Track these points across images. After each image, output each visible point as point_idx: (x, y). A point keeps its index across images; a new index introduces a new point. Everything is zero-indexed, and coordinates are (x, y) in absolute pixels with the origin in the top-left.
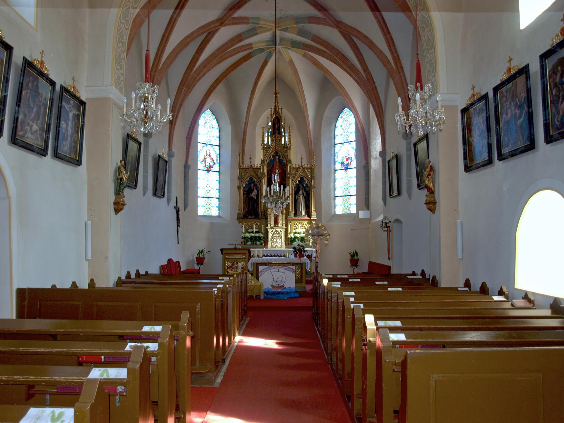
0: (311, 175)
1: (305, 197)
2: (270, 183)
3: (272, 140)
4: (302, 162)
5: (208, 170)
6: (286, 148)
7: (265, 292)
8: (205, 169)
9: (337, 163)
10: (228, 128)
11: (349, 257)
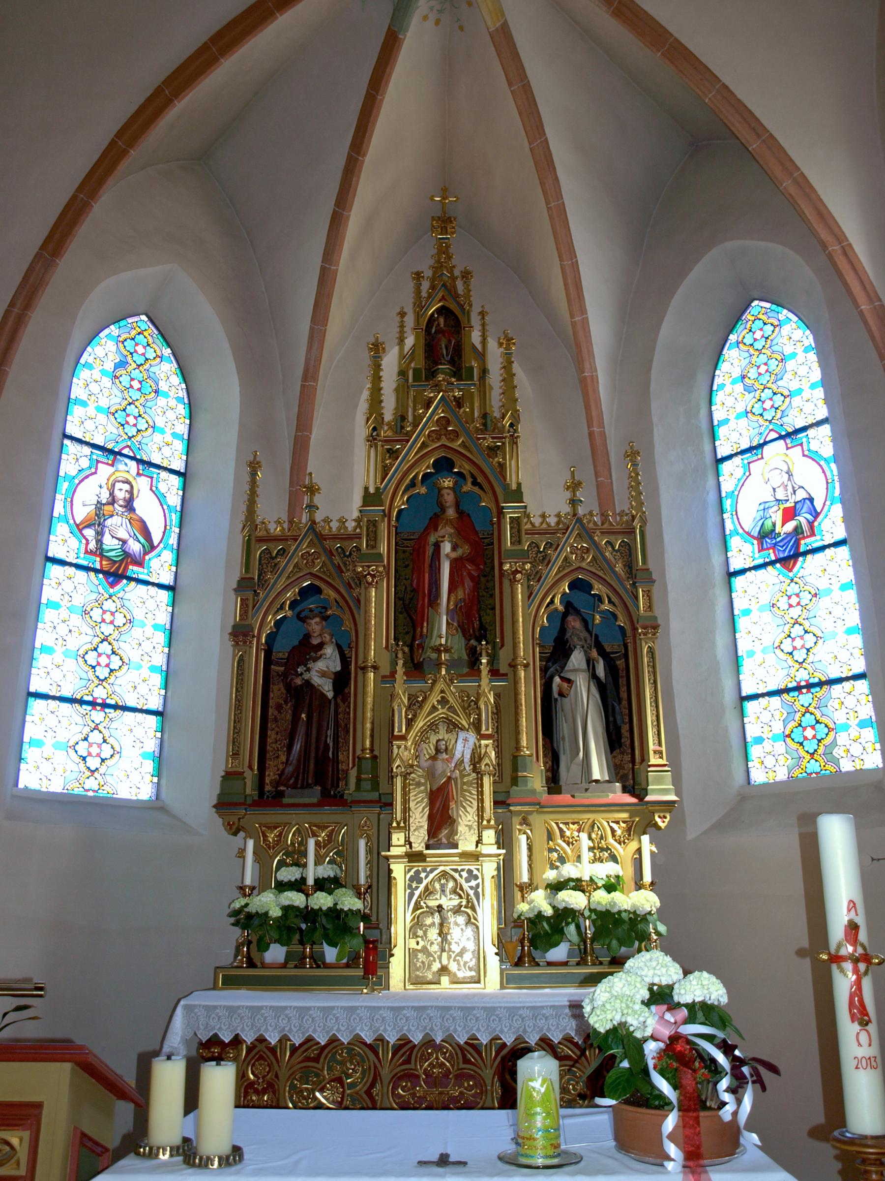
1: (602, 688)
4: (574, 502)
5: (116, 571)
9: (735, 543)
10: (228, 391)
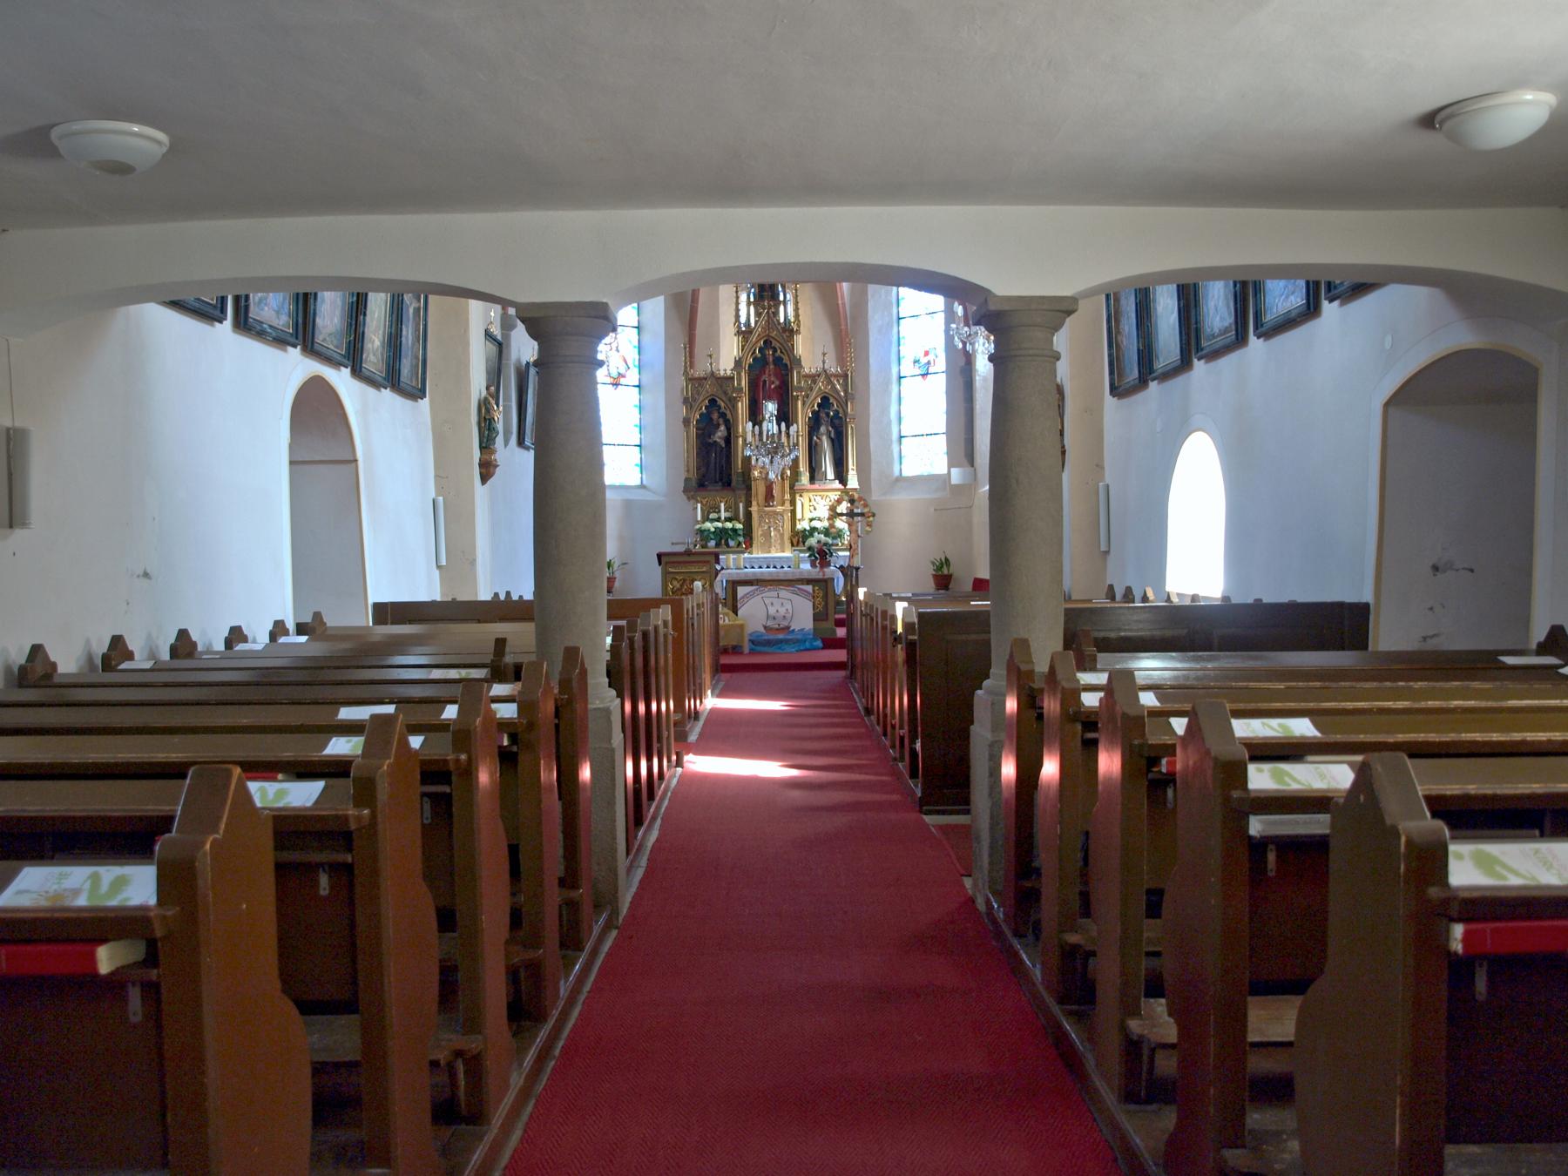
0: (846, 391)
1: (832, 440)
2: (755, 415)
3: (758, 314)
6: (789, 331)
7: (752, 642)
8: (609, 380)
11: (931, 571)
